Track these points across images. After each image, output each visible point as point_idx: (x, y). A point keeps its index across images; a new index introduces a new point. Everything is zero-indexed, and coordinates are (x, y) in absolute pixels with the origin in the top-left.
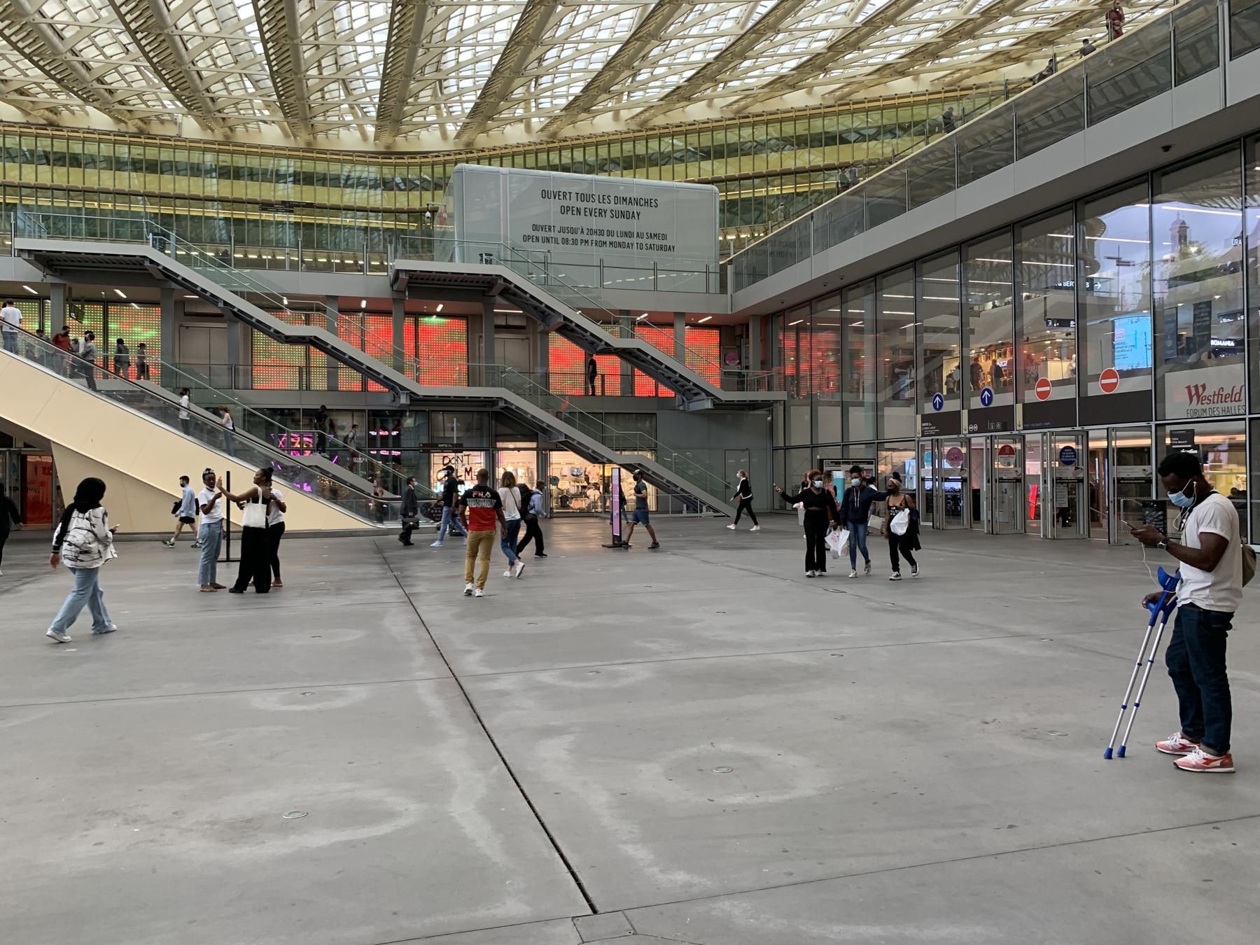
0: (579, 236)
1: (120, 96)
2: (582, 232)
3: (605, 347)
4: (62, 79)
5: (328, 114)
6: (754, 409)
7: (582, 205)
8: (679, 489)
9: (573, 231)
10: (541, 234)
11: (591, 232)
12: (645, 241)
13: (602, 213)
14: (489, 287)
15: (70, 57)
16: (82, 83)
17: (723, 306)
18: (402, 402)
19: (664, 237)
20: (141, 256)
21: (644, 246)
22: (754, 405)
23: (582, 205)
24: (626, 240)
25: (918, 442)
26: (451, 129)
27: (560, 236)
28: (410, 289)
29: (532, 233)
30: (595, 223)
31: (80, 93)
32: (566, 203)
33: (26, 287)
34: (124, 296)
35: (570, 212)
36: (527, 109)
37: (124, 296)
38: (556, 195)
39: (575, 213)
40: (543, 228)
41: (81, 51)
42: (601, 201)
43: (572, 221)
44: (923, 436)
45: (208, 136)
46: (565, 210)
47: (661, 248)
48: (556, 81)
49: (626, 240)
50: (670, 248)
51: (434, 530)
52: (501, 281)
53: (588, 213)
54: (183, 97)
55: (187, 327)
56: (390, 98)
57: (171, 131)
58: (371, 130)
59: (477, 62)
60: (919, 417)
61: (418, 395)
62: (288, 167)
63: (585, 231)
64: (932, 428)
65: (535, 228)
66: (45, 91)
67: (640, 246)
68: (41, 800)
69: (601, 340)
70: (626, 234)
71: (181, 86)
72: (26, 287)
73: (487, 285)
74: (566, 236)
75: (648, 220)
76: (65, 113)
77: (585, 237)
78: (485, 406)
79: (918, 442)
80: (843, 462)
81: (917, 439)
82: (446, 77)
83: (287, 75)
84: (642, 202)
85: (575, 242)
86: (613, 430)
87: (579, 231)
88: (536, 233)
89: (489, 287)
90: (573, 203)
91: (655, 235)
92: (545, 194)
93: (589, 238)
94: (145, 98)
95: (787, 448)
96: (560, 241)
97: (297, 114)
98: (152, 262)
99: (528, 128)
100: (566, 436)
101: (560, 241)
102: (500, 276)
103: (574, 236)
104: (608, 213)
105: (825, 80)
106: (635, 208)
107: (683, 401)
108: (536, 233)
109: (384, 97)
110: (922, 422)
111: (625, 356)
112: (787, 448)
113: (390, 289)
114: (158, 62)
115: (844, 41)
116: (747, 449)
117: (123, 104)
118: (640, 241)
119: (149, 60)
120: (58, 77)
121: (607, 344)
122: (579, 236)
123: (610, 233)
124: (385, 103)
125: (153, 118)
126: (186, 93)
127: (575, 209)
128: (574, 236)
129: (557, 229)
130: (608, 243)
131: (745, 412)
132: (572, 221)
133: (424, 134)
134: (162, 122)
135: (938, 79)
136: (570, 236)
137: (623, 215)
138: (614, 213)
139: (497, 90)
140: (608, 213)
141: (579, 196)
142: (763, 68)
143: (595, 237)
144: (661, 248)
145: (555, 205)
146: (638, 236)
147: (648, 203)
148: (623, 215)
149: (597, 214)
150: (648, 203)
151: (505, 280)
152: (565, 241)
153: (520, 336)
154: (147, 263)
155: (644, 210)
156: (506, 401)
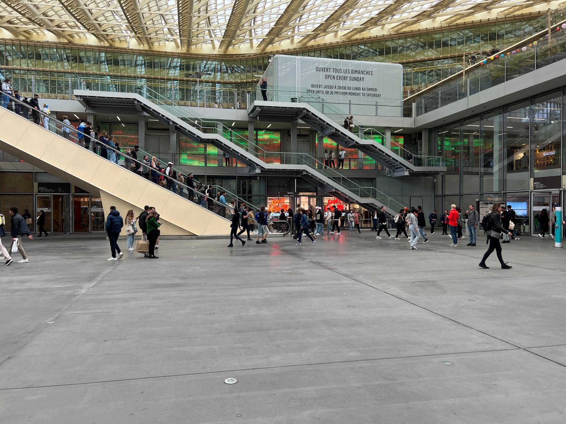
0: (334, 90)
1: (104, 27)
2: (335, 88)
3: (356, 144)
4: (79, 19)
5: (199, 36)
6: (426, 176)
7: (336, 74)
8: (391, 216)
9: (331, 87)
10: (315, 89)
11: (340, 88)
12: (366, 92)
13: (345, 78)
14: (296, 115)
15: (85, 7)
16: (88, 21)
17: (407, 123)
18: (257, 172)
19: (376, 90)
20: (133, 99)
21: (366, 94)
22: (425, 174)
23: (336, 74)
24: (357, 92)
25: (531, 192)
26: (256, 43)
27: (325, 90)
28: (260, 116)
29: (311, 89)
30: (342, 83)
31: (86, 26)
32: (328, 73)
33: (75, 115)
34: (120, 120)
35: (330, 78)
36: (293, 32)
37: (120, 120)
38: (323, 70)
39: (332, 78)
40: (316, 86)
41: (89, 5)
42: (345, 72)
43: (330, 82)
44: (534, 189)
45: (141, 47)
46: (327, 77)
47: (374, 95)
48: (310, 17)
49: (357, 92)
50: (379, 96)
51: (283, 236)
52: (305, 111)
53: (338, 78)
54: (134, 28)
55: (148, 135)
56: (232, 26)
57: (124, 45)
58: (217, 44)
59: (273, 8)
60: (532, 180)
61: (265, 169)
62: (141, 72)
63: (337, 87)
64: (541, 185)
65: (313, 86)
66: (69, 26)
67: (364, 95)
68: (190, 396)
69: (354, 140)
70: (357, 89)
71: (133, 22)
72: (75, 115)
73: (296, 114)
74: (327, 90)
75: (368, 82)
76: (76, 37)
77: (337, 90)
78: (292, 174)
79: (531, 192)
80: (490, 203)
81: (530, 191)
82: (215, 29)
83: (186, 15)
84: (365, 73)
85: (332, 93)
86: (360, 187)
87: (334, 87)
88: (313, 89)
89: (296, 115)
90: (332, 73)
91: (371, 89)
92: (318, 69)
93: (339, 91)
94: (114, 29)
95: (443, 196)
96: (324, 92)
97: (186, 35)
98: (138, 101)
99: (292, 42)
100: (336, 189)
101: (324, 92)
102: (304, 109)
103: (332, 90)
104: (348, 79)
105: (442, 14)
106: (361, 76)
107: (390, 172)
108: (313, 89)
109: (229, 26)
110: (534, 182)
111: (362, 149)
112: (443, 196)
113: (248, 116)
114: (126, 9)
115: (385, 11)
116: (421, 196)
117: (105, 32)
118: (364, 92)
119: (122, 7)
120: (78, 18)
121: (356, 142)
122: (334, 90)
123: (349, 88)
124: (229, 29)
125: (117, 39)
126: (136, 25)
127: (332, 76)
128: (332, 90)
129: (323, 86)
130: (348, 93)
131: (420, 177)
132: (330, 82)
133: (242, 45)
134: (121, 41)
135: (501, 12)
136: (329, 90)
137: (355, 79)
138: (351, 78)
139: (284, 21)
140: (348, 79)
141: (334, 70)
142: (413, 8)
143: (341, 90)
144: (374, 95)
145: (322, 74)
146: (363, 89)
147: (368, 73)
148: (355, 79)
149: (343, 79)
150: (368, 73)
151: (307, 110)
152: (327, 93)
153: (305, 140)
154: (136, 102)
155: (366, 76)
156: (307, 172)
